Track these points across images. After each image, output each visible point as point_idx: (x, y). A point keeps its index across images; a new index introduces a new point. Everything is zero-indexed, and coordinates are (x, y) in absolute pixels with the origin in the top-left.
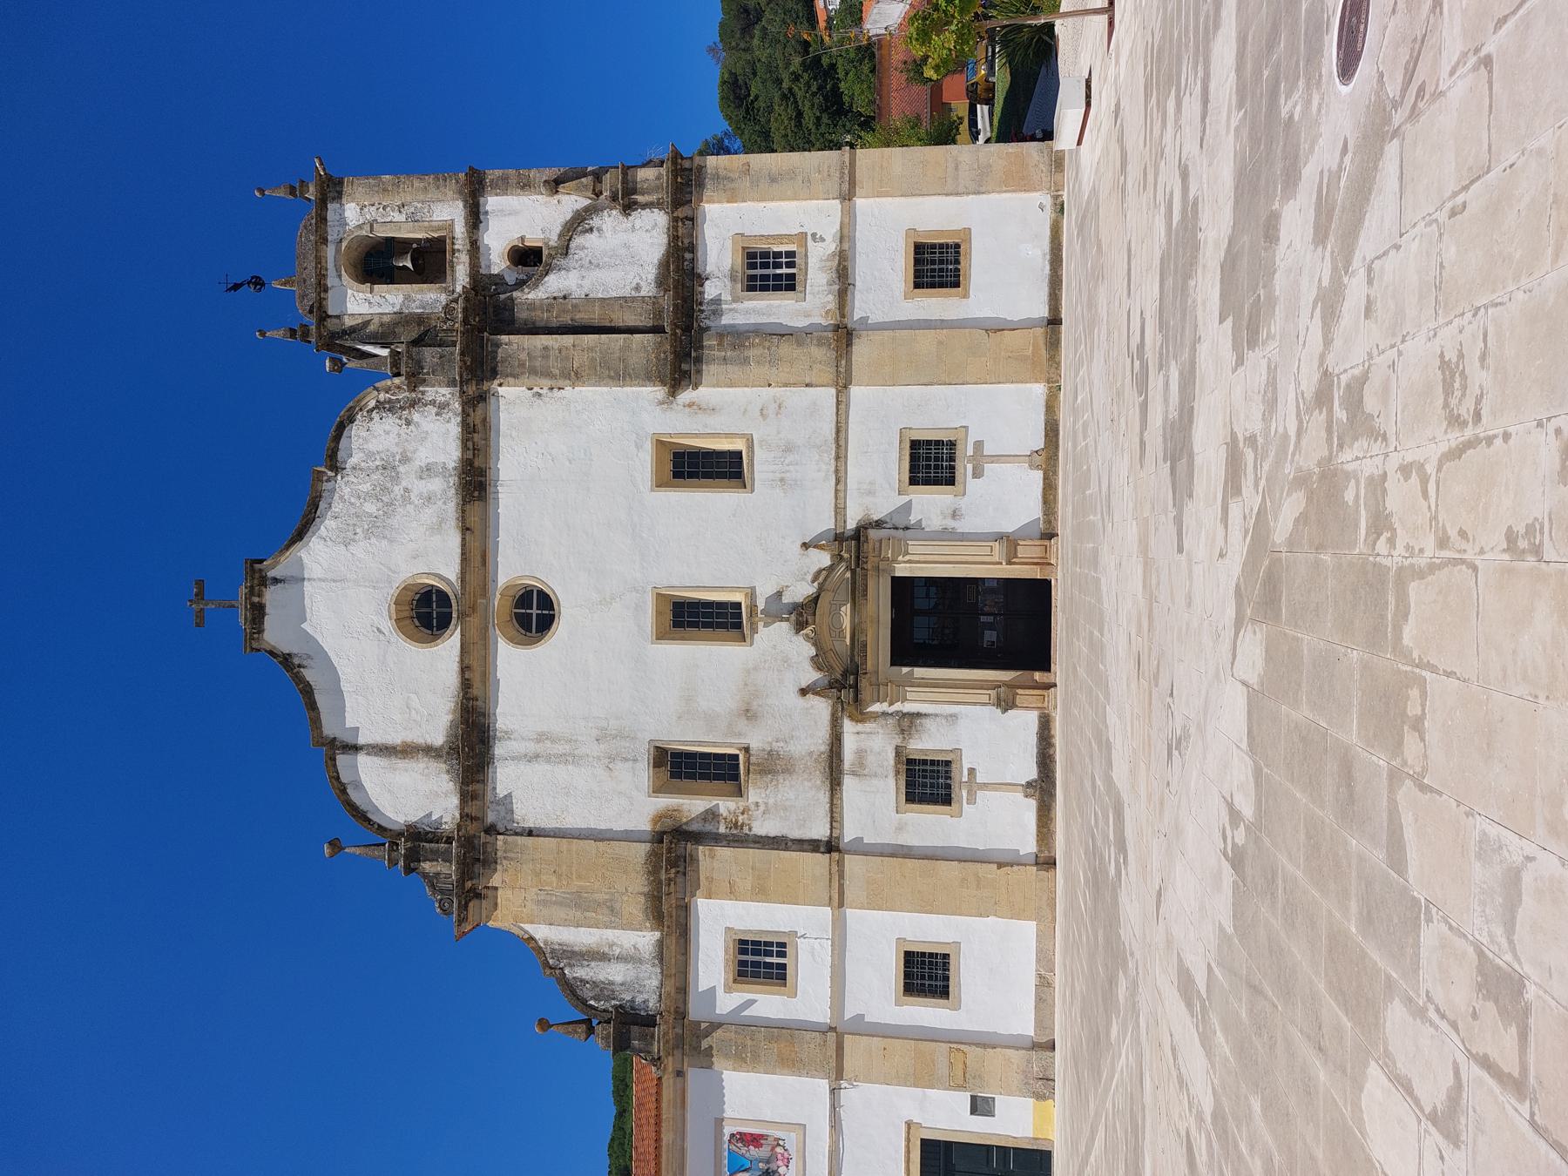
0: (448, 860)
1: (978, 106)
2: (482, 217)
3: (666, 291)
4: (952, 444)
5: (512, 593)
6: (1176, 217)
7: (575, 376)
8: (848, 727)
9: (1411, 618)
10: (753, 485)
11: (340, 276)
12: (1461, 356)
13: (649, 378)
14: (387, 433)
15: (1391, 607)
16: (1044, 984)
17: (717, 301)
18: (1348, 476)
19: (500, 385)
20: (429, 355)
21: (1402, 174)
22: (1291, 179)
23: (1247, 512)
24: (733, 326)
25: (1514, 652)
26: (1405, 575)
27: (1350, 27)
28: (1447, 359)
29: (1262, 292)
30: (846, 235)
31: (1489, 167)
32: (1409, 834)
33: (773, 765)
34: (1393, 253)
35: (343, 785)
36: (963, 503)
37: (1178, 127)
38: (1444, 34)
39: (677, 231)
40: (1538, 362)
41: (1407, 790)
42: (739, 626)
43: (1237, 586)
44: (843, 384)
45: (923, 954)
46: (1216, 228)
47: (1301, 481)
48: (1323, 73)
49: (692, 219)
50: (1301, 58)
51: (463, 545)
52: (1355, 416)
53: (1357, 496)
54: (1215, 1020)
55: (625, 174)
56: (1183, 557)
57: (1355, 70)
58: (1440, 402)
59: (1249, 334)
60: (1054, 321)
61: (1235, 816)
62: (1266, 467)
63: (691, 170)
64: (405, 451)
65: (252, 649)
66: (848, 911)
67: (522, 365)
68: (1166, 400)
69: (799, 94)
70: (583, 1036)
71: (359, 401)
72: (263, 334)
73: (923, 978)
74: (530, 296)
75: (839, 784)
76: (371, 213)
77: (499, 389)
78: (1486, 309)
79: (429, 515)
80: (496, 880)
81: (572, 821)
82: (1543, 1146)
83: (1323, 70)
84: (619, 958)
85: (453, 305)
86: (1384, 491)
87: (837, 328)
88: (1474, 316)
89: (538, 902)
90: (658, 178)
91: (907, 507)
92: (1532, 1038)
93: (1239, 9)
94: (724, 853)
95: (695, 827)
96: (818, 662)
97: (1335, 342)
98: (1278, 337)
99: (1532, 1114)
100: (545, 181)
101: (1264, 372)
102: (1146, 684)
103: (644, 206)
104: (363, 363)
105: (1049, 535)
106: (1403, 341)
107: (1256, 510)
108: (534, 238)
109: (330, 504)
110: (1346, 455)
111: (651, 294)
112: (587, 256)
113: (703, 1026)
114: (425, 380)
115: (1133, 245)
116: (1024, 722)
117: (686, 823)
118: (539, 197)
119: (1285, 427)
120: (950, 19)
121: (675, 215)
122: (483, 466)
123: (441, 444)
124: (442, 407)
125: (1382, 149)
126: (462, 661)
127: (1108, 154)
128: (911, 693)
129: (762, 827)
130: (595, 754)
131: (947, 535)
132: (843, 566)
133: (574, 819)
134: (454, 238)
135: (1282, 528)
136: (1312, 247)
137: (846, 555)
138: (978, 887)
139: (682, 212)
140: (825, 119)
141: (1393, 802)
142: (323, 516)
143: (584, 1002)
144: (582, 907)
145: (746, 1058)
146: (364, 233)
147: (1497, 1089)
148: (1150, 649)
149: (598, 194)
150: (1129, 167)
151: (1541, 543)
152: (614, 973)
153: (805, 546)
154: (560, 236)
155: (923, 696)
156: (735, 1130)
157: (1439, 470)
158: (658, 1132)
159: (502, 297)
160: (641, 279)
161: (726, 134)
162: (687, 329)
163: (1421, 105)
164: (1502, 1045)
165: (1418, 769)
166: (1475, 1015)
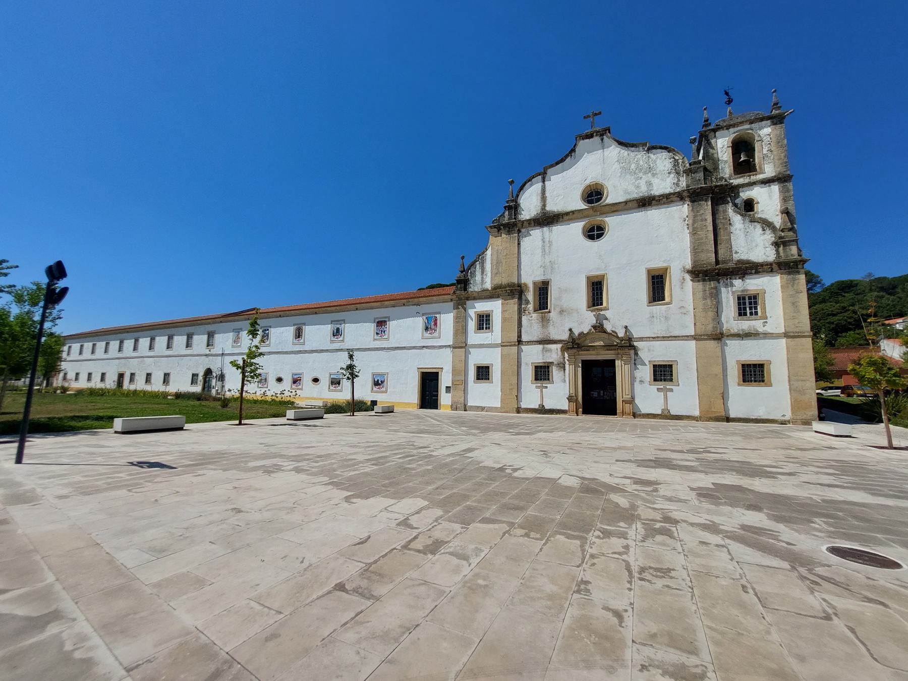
0: (509, 219)
1: (840, 390)
2: (767, 184)
3: (736, 264)
4: (671, 380)
5: (602, 224)
6: (768, 469)
7: (694, 233)
8: (559, 346)
9: (567, 540)
10: (650, 306)
11: (734, 133)
12: (672, 578)
13: (695, 262)
14: (665, 166)
15: (573, 533)
16: (482, 409)
17: (732, 285)
18: (630, 525)
19: (688, 205)
20: (700, 175)
21: (771, 567)
22: (779, 519)
23: (626, 486)
24: (721, 293)
25: (542, 575)
26: (583, 540)
27: (861, 555)
28: (672, 571)
29: (723, 501)
30: (767, 336)
31: (765, 607)
32: (491, 526)
33: (545, 321)
34: (730, 557)
35: (531, 180)
36: (647, 385)
37: (817, 473)
38: (850, 600)
39: (765, 266)
40: (660, 609)
41: (505, 527)
42: (594, 305)
43: (597, 479)
44: (696, 338)
45: (489, 372)
46: (760, 485)
47: (633, 507)
48: (836, 540)
49: (772, 271)
50: (847, 531)
51: (620, 203)
52: (655, 531)
53: (621, 527)
54: (457, 457)
55: (793, 241)
56: (614, 462)
57: (835, 555)
58: (652, 565)
59: (704, 494)
60: (728, 419)
61: (515, 470)
62: (642, 494)
63: (797, 268)
64: (657, 174)
65: (576, 138)
66: (500, 348)
67: (698, 212)
68: (682, 460)
69: (846, 314)
70: (460, 270)
71: (678, 153)
72: (705, 109)
73: (482, 372)
74: (730, 210)
75: (540, 344)
76: (766, 139)
77: (687, 205)
78: (691, 592)
79: (631, 188)
80: (504, 236)
81: (523, 257)
82: (387, 551)
83: (837, 540)
84: (482, 278)
85: (724, 180)
86: (620, 538)
87: (722, 334)
88: (689, 587)
89: (498, 250)
90: (792, 255)
91: (644, 364)
92: (417, 554)
93: (882, 505)
94: (516, 307)
95: (523, 297)
96: (581, 334)
97: (691, 528)
98: (700, 505)
99: (397, 549)
100: (787, 208)
101: (685, 498)
102: (570, 445)
103: (777, 251)
104: (695, 151)
105: (635, 415)
106: (684, 555)
107: (626, 489)
108: (758, 208)
109: (634, 151)
110: (639, 525)
111: (734, 258)
112: (751, 230)
113: (465, 306)
114: (689, 175)
115: (759, 451)
116: (565, 405)
117: (524, 294)
118: (779, 207)
119: (658, 503)
120: (883, 375)
121: (774, 264)
122: (653, 204)
123: (661, 187)
124: (677, 185)
125: (786, 561)
126: (576, 211)
127: (809, 443)
128: (572, 367)
129: (524, 319)
130: (546, 261)
131: (633, 379)
132: (619, 341)
133: (524, 258)
134: (756, 175)
135: (616, 498)
136: (740, 523)
137: (623, 342)
138: (510, 389)
139: (775, 266)
140: (832, 326)
141: (503, 522)
142: (628, 150)
143: (470, 269)
144: (497, 264)
145: (457, 318)
146: (756, 138)
147: (407, 540)
148: (582, 447)
149: (782, 231)
150: (800, 452)
151: (581, 594)
152: (478, 277)
153: (626, 327)
154: (760, 218)
155: (571, 371)
156: (438, 318)
157: (623, 560)
158: (436, 296)
159: (729, 199)
160: (741, 254)
161: (823, 285)
162: (718, 274)
163: (808, 582)
164: (418, 545)
165: (511, 533)
166: (430, 537)
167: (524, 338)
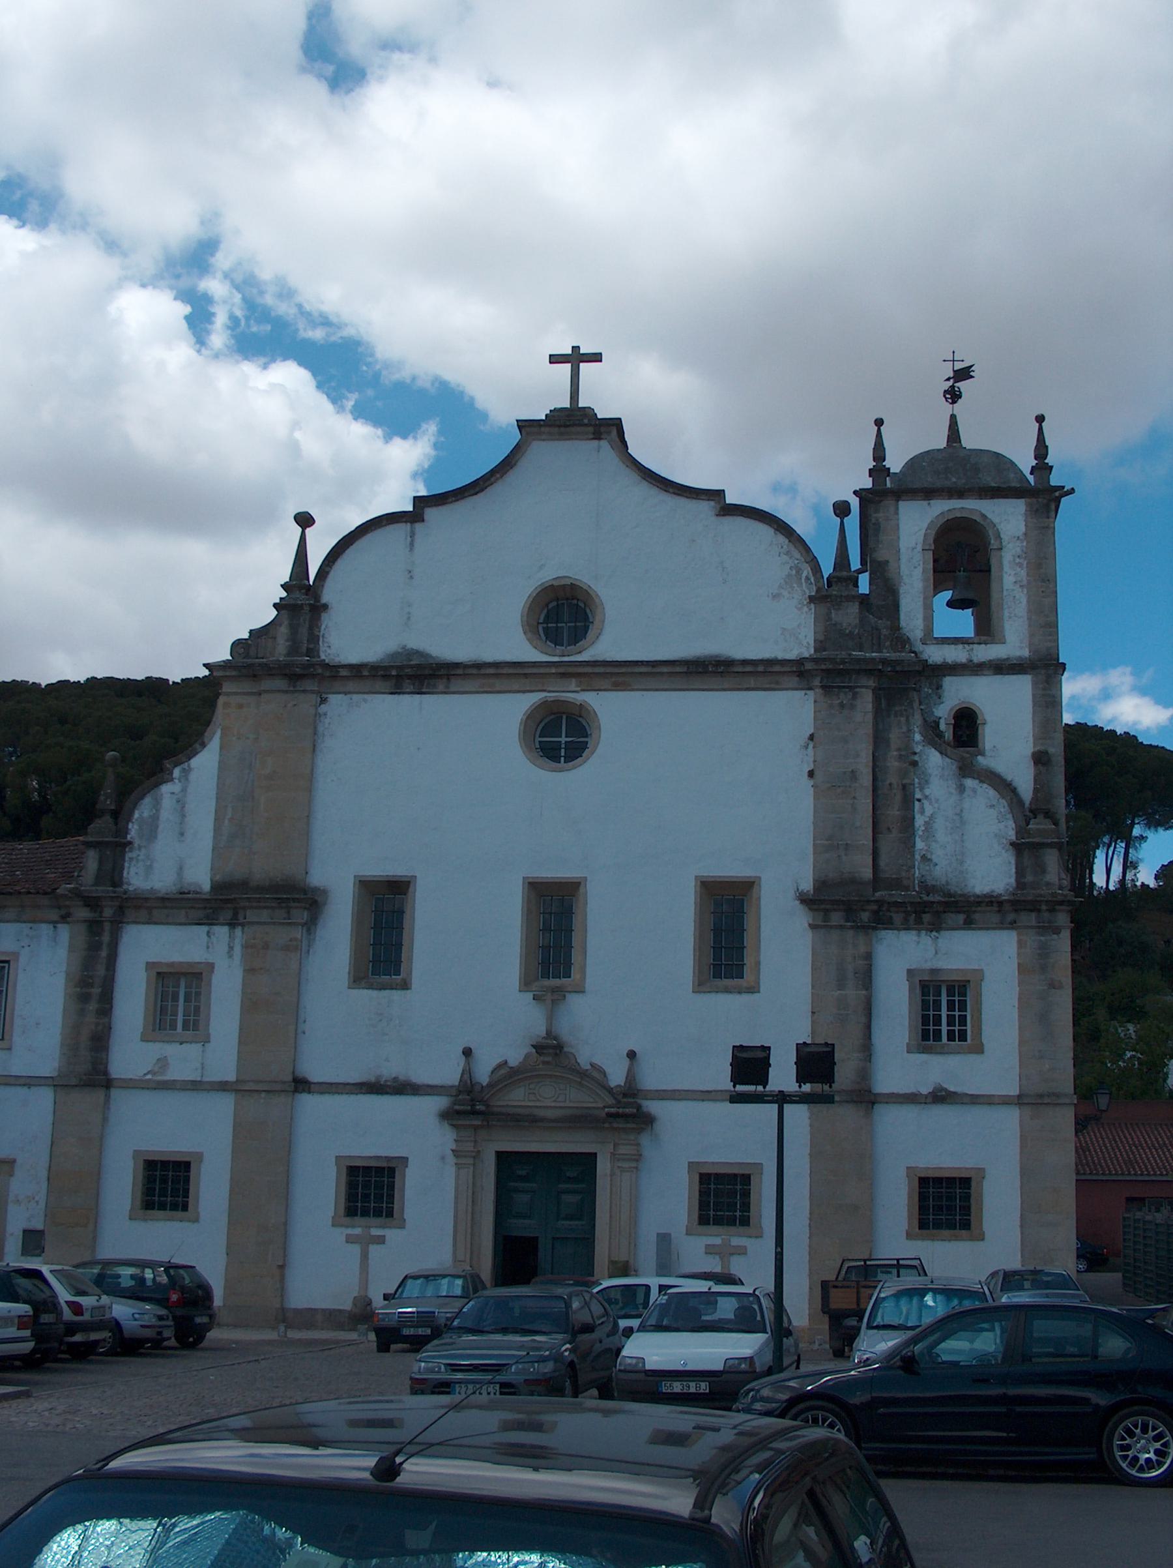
108: (989, 736)
167: (788, 1108)
